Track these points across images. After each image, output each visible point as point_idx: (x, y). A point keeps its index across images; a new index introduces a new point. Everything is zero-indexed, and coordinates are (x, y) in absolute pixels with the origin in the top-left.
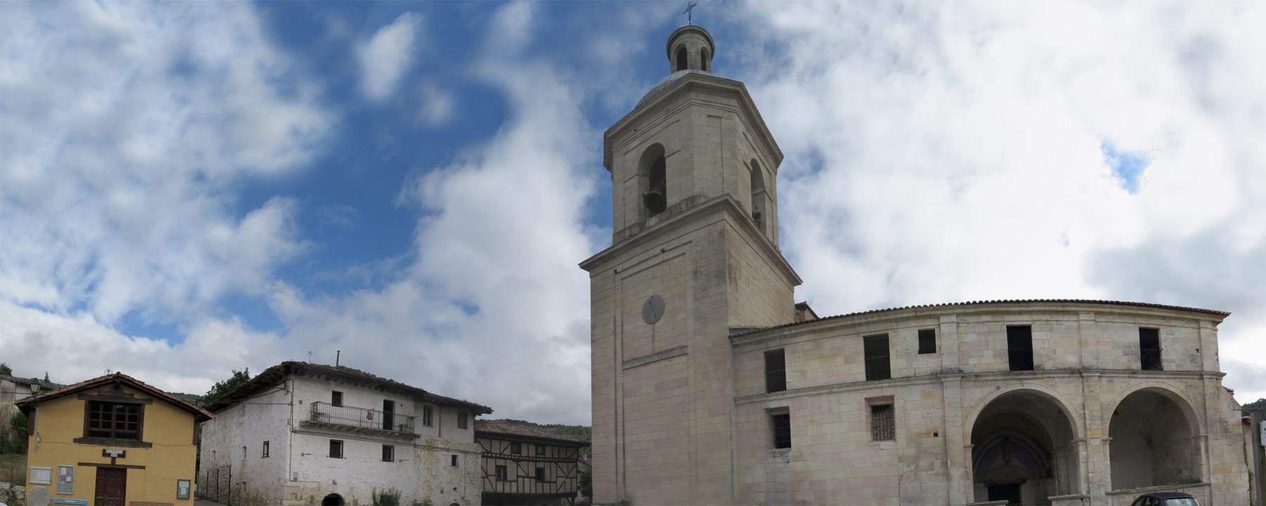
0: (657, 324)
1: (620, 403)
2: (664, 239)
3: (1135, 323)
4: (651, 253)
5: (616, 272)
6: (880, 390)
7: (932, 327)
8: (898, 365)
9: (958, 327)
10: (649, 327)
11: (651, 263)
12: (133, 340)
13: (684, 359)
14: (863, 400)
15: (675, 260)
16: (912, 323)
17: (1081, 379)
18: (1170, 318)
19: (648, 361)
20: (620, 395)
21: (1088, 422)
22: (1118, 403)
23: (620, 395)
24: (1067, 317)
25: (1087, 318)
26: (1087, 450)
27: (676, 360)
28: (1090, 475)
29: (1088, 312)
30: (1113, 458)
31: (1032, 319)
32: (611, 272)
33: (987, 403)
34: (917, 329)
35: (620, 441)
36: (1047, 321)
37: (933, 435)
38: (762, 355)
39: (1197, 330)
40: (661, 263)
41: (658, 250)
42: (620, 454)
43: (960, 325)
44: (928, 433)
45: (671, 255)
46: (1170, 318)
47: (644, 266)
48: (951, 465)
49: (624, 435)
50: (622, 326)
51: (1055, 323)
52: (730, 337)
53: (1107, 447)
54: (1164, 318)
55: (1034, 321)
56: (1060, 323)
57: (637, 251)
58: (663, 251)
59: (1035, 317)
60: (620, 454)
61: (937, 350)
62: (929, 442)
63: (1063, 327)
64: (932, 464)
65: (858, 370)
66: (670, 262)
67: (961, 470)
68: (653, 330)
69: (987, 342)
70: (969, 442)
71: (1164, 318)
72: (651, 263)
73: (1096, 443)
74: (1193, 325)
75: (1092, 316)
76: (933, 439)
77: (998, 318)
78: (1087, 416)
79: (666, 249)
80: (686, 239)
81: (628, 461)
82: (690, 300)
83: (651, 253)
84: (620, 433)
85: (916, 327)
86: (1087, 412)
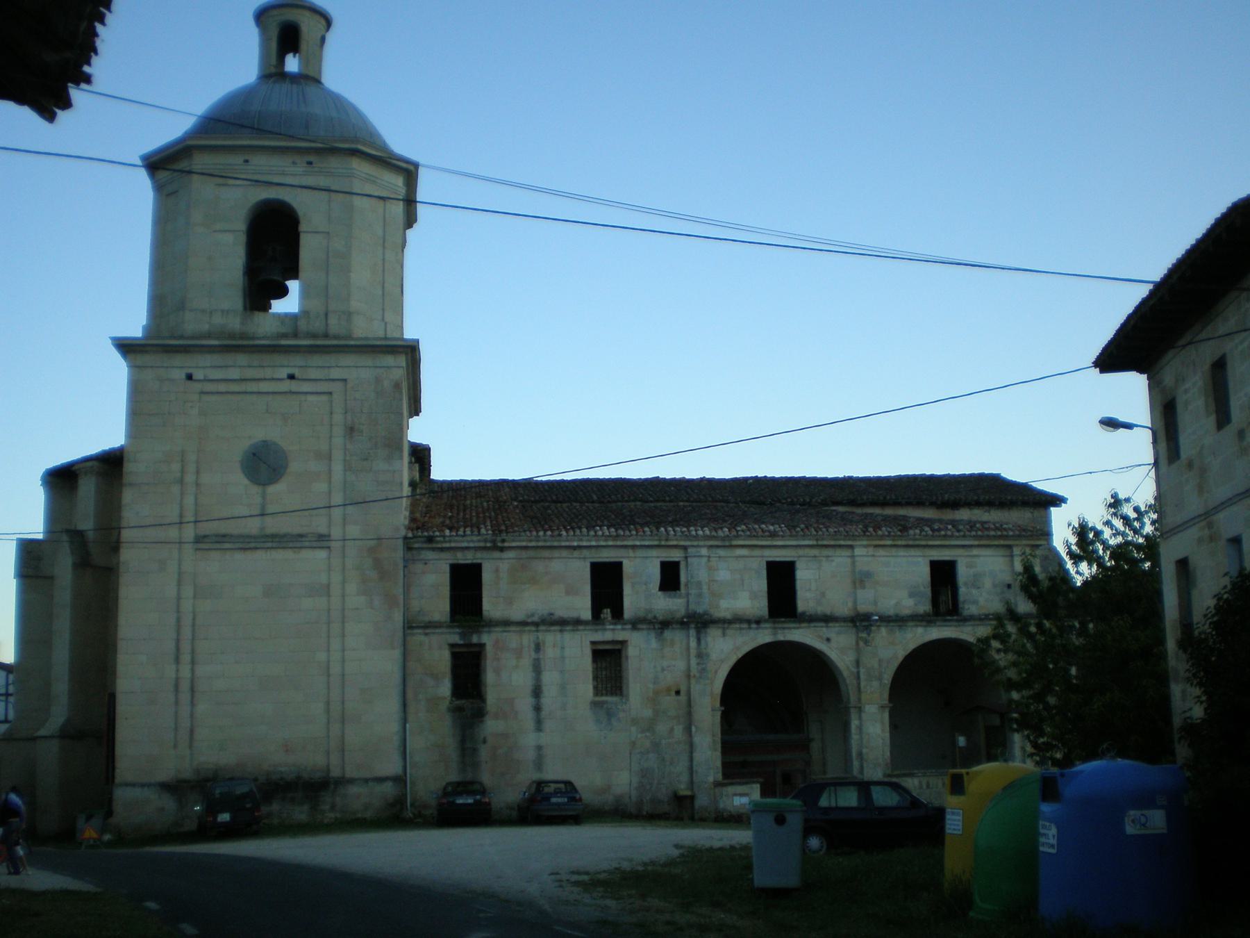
0: (271, 489)
1: (187, 606)
2: (298, 360)
3: (924, 556)
4: (268, 373)
5: (190, 377)
6: (610, 633)
7: (677, 560)
8: (632, 601)
9: (709, 561)
10: (255, 489)
11: (264, 387)
12: (677, 846)
13: (322, 554)
14: (588, 643)
15: (311, 398)
16: (654, 553)
17: (854, 629)
18: (971, 546)
19: (252, 545)
20: (188, 591)
21: (863, 684)
22: (901, 658)
23: (188, 591)
24: (839, 552)
25: (865, 553)
26: (860, 718)
27: (306, 554)
28: (864, 751)
29: (866, 546)
30: (894, 726)
31: (796, 555)
32: (179, 374)
33: (740, 655)
34: (659, 560)
35: (185, 672)
36: (815, 557)
37: (674, 693)
38: (447, 569)
39: (1007, 559)
40: (285, 393)
41: (283, 373)
42: (185, 697)
43: (711, 559)
44: (668, 690)
45: (306, 387)
46: (971, 546)
47: (252, 387)
48: (696, 732)
49: (193, 663)
50: (198, 472)
51: (824, 559)
52: (405, 538)
53: (886, 715)
54: (963, 546)
55: (799, 557)
56: (830, 559)
57: (242, 359)
58: (291, 377)
59: (801, 552)
60: (185, 697)
61: (682, 587)
62: (669, 701)
63: (834, 564)
64: (672, 730)
65: (582, 606)
66: (303, 397)
67: (708, 739)
68: (264, 496)
69: (743, 581)
70: (718, 704)
71: (963, 546)
72: (264, 387)
73: (871, 709)
74: (1002, 552)
75: (871, 551)
76: (673, 697)
77: (757, 552)
78: (862, 676)
79: (297, 375)
80: (335, 373)
81: (201, 707)
82: (338, 468)
83: (268, 373)
84: (186, 658)
85: (658, 557)
86: (862, 670)
